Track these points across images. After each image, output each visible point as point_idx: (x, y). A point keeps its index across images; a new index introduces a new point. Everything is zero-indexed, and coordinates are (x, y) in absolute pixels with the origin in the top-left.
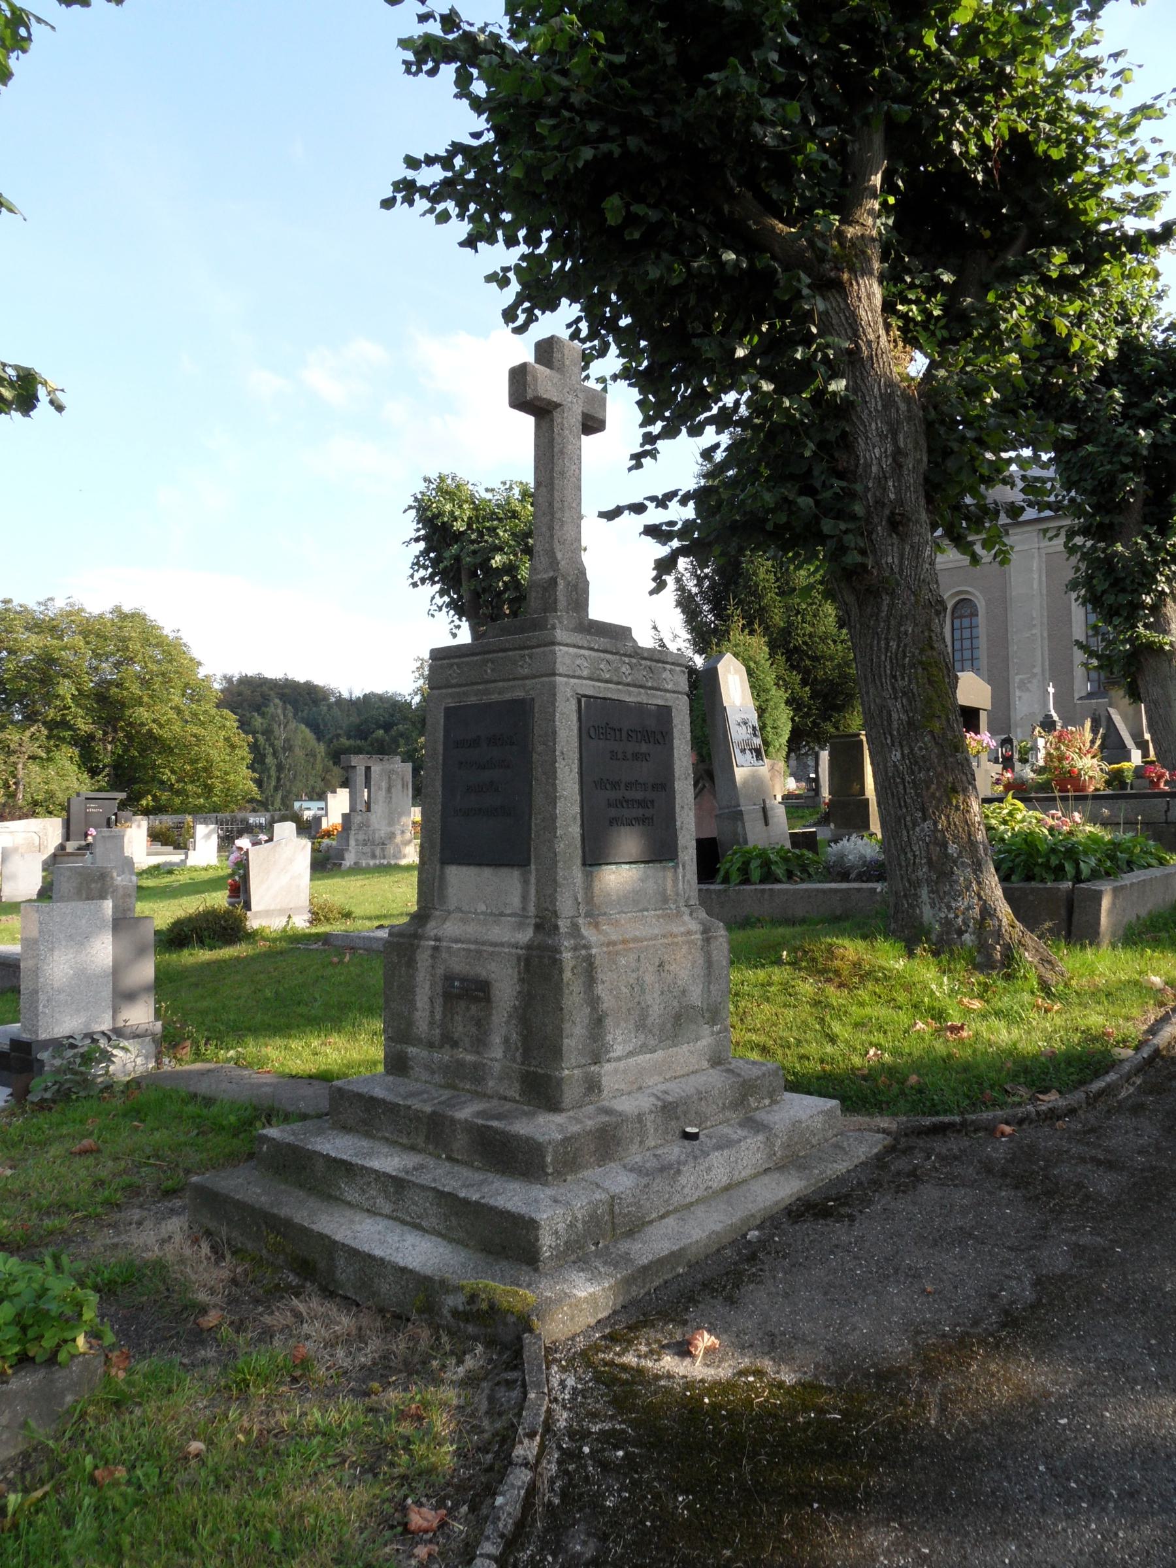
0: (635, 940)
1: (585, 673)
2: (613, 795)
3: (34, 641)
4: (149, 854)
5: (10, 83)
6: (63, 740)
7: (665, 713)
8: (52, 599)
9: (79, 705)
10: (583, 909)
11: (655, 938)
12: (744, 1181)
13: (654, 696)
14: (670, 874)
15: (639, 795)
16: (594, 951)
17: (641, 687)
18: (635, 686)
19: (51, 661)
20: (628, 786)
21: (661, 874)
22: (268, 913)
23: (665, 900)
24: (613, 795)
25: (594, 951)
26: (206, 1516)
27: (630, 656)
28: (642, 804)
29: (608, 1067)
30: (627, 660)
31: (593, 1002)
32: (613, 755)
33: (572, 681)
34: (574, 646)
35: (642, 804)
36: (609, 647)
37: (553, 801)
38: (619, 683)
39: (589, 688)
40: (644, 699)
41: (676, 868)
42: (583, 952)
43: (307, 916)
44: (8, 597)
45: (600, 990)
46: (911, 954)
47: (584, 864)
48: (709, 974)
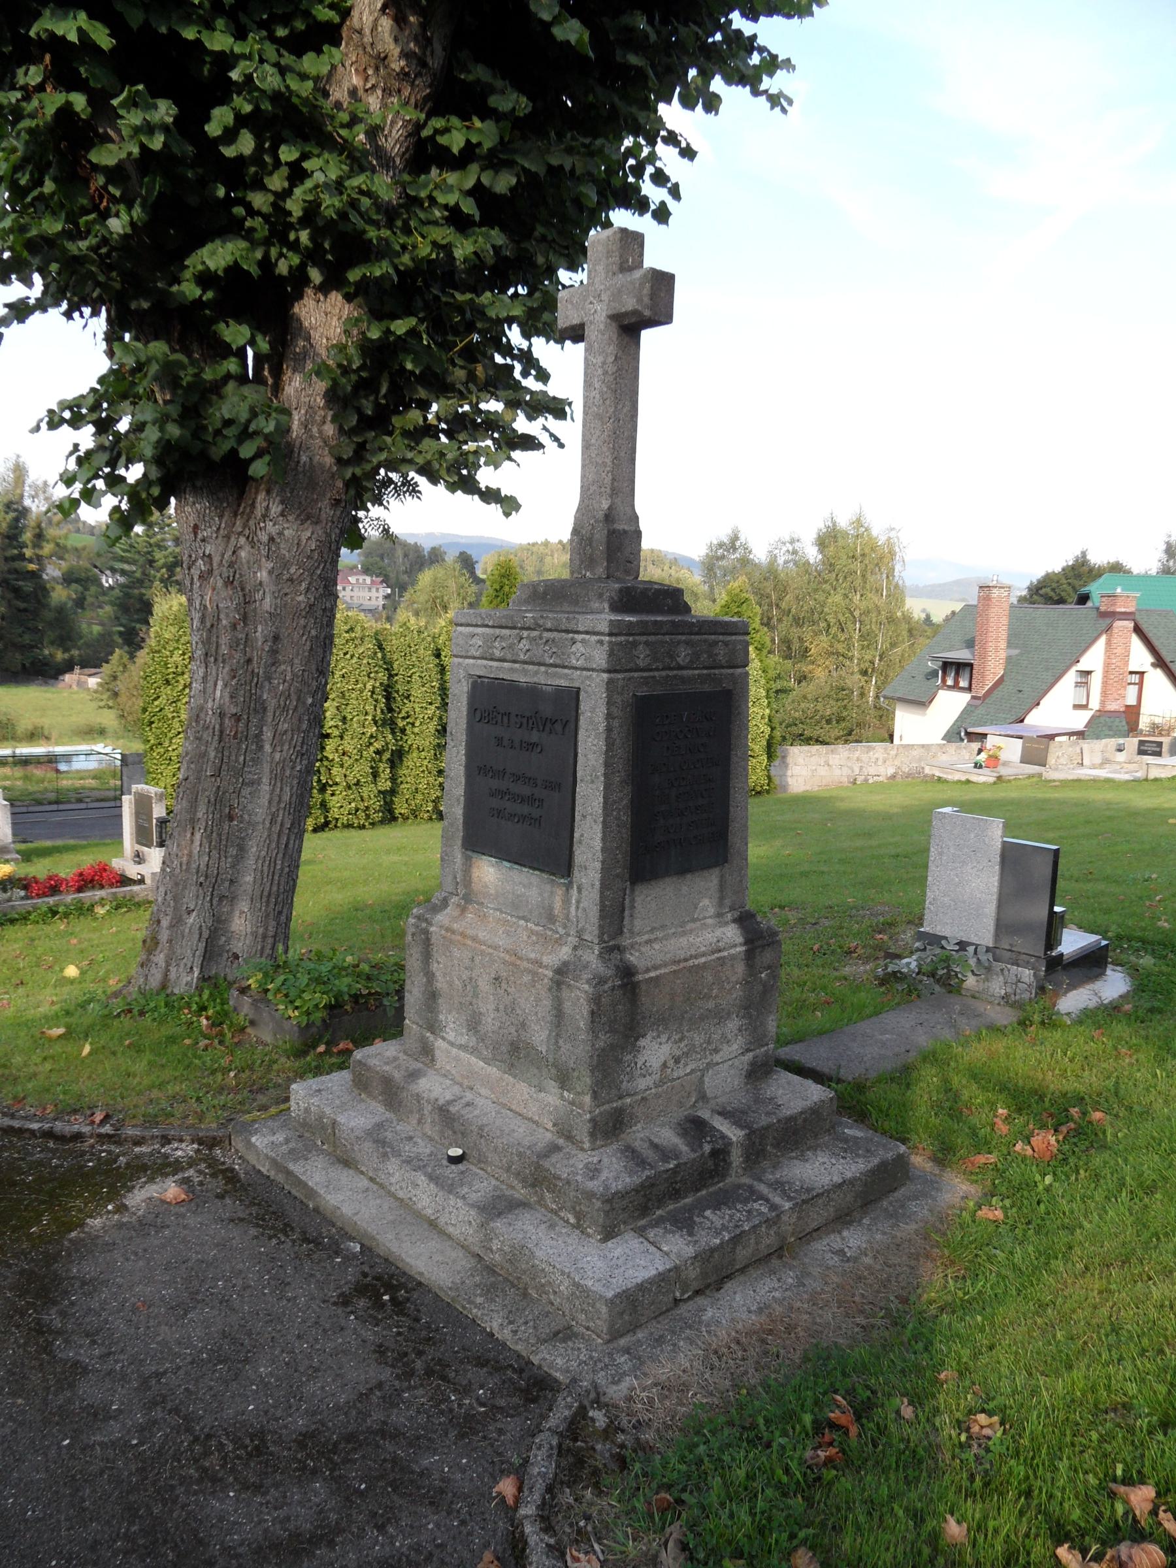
0: (474, 939)
2: (495, 784)
5: (722, 108)
7: (572, 697)
10: (462, 891)
11: (496, 948)
12: (449, 1237)
13: (555, 675)
14: (560, 892)
15: (526, 790)
16: (432, 929)
17: (540, 664)
18: (533, 663)
20: (517, 778)
21: (548, 887)
23: (552, 919)
24: (495, 784)
25: (432, 929)
28: (530, 800)
30: (525, 633)
31: (430, 976)
32: (499, 741)
34: (468, 625)
35: (530, 800)
37: (746, 758)
38: (514, 662)
39: (481, 667)
40: (542, 679)
41: (569, 886)
42: (424, 925)
45: (434, 967)
46: (334, 1123)
48: (558, 1025)
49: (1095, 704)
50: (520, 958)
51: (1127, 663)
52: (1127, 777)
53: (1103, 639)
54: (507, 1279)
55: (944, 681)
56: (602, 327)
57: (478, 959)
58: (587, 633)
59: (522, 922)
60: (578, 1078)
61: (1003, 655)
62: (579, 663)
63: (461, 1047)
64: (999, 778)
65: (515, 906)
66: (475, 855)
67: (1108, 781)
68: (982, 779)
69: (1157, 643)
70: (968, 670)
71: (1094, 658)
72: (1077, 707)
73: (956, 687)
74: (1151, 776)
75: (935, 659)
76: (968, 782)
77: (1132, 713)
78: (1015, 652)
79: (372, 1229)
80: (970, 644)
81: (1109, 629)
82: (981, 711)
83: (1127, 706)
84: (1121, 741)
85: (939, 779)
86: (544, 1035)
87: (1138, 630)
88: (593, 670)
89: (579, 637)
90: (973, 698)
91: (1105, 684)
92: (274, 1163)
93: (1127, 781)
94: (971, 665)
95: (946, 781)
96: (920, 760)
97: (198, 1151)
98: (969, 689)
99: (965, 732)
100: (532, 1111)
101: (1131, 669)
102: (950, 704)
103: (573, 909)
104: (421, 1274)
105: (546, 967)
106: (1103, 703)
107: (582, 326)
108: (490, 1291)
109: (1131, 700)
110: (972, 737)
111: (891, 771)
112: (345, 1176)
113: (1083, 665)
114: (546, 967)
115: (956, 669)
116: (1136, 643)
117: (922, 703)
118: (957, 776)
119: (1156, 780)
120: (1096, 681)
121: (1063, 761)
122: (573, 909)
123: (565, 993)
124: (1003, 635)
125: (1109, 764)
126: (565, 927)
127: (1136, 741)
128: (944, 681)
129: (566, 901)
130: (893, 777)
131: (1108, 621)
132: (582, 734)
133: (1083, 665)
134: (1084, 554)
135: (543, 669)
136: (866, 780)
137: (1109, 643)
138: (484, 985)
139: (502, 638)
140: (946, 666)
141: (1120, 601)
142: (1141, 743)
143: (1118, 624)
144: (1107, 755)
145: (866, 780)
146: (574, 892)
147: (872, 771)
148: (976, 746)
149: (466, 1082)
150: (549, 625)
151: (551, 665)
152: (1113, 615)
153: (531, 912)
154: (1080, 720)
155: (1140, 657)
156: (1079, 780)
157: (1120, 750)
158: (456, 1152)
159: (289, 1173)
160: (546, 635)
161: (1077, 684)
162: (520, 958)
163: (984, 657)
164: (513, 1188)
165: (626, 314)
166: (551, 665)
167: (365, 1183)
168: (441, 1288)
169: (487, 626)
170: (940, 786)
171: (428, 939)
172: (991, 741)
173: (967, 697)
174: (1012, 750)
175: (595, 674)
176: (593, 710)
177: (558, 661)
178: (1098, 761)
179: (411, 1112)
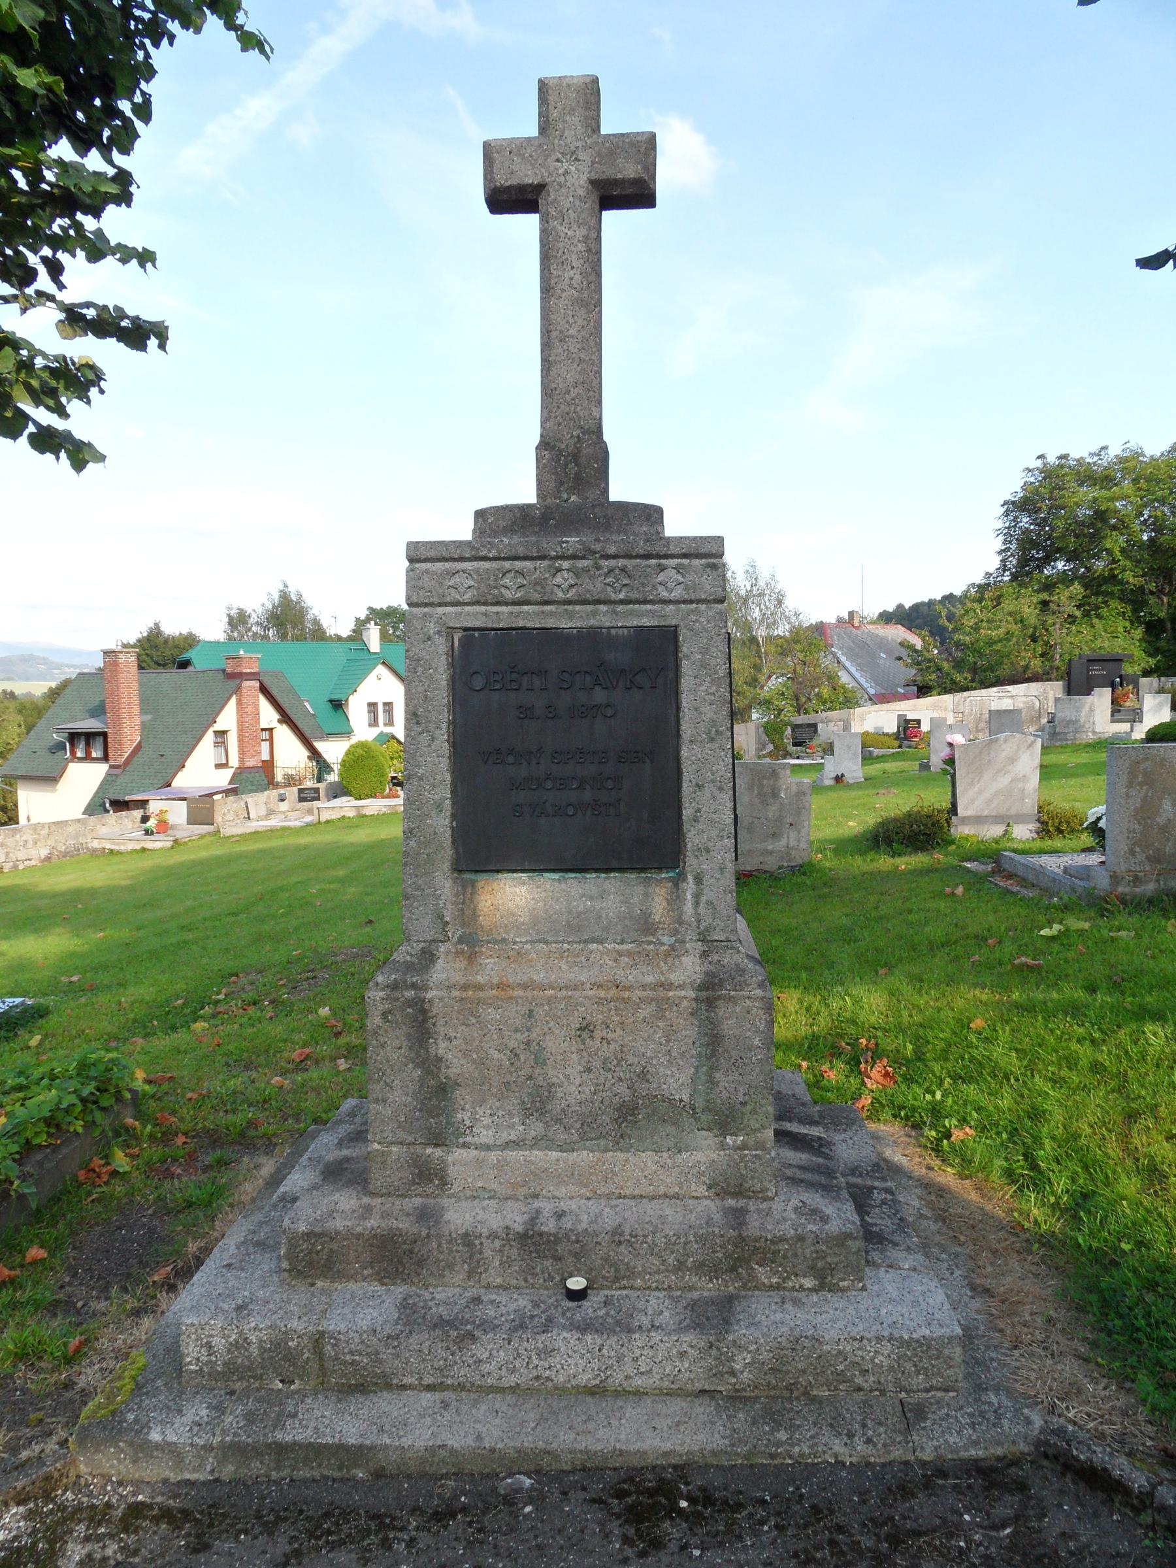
1: (468, 597)
3: (1087, 493)
4: (1113, 721)
6: (1112, 594)
8: (1104, 448)
9: (1128, 558)
10: (455, 932)
12: (639, 1394)
13: (630, 614)
18: (584, 602)
19: (1101, 516)
21: (640, 889)
22: (979, 820)
26: (21, 1467)
27: (574, 557)
29: (459, 1154)
30: (566, 564)
33: (440, 610)
36: (521, 551)
41: (677, 882)
43: (1034, 826)
44: (1064, 452)
47: (458, 868)
49: (234, 762)
50: (626, 988)
51: (258, 721)
52: (298, 824)
53: (233, 701)
54: (786, 1389)
55: (73, 753)
56: (582, 192)
57: (539, 1012)
58: (685, 556)
59: (594, 946)
60: (754, 1112)
61: (137, 721)
62: (674, 595)
63: (508, 1145)
64: (176, 841)
65: (578, 931)
66: (480, 876)
67: (284, 829)
68: (158, 845)
69: (280, 701)
70: (100, 740)
71: (228, 719)
72: (219, 766)
73: (88, 758)
74: (323, 819)
75: (59, 731)
76: (144, 850)
77: (268, 766)
78: (149, 717)
79: (528, 1441)
80: (99, 711)
81: (239, 688)
82: (123, 779)
83: (263, 761)
84: (282, 791)
85: (111, 851)
86: (685, 1076)
87: (264, 690)
88: (699, 601)
89: (673, 562)
90: (112, 767)
91: (241, 741)
92: (236, 1451)
93: (302, 827)
94: (104, 735)
95: (119, 853)
96: (77, 836)
97: (29, 1516)
98: (106, 758)
99: (112, 803)
100: (669, 1182)
101: (263, 726)
102: (84, 778)
103: (689, 908)
104: (666, 1454)
105: (681, 987)
106: (241, 760)
107: (540, 188)
108: (773, 1417)
109: (265, 756)
110: (120, 805)
111: (44, 853)
112: (385, 1404)
113: (218, 727)
114: (681, 987)
115: (88, 741)
116: (263, 703)
117: (50, 779)
118: (131, 846)
119: (328, 822)
120: (233, 740)
121: (230, 817)
122: (689, 908)
123: (722, 1010)
124: (135, 700)
125: (264, 815)
126: (675, 932)
127: (295, 789)
128: (73, 753)
129: (676, 900)
130: (48, 858)
131: (237, 682)
132: (686, 684)
133: (218, 727)
134: (157, 625)
135: (603, 608)
136: (15, 867)
137: (239, 703)
138: (557, 1043)
139: (520, 573)
140: (73, 737)
141: (245, 662)
142: (301, 791)
143: (246, 684)
144: (271, 806)
145: (15, 867)
146: (689, 887)
147: (21, 855)
148: (138, 814)
149: (522, 1192)
150: (612, 550)
151: (622, 602)
152: (241, 676)
153: (606, 929)
154: (223, 779)
155: (268, 715)
156: (256, 833)
157: (282, 800)
158: (576, 1283)
159: (281, 1449)
160: (605, 563)
161: (216, 744)
162: (626, 988)
163: (118, 723)
164: (691, 1288)
165: (615, 183)
166: (622, 602)
167: (427, 1398)
168: (714, 1453)
169: (485, 558)
170: (116, 859)
171: (423, 1012)
172: (154, 807)
173: (103, 768)
174: (178, 813)
175: (703, 607)
176: (705, 651)
177: (634, 595)
178: (263, 812)
179: (451, 1266)
